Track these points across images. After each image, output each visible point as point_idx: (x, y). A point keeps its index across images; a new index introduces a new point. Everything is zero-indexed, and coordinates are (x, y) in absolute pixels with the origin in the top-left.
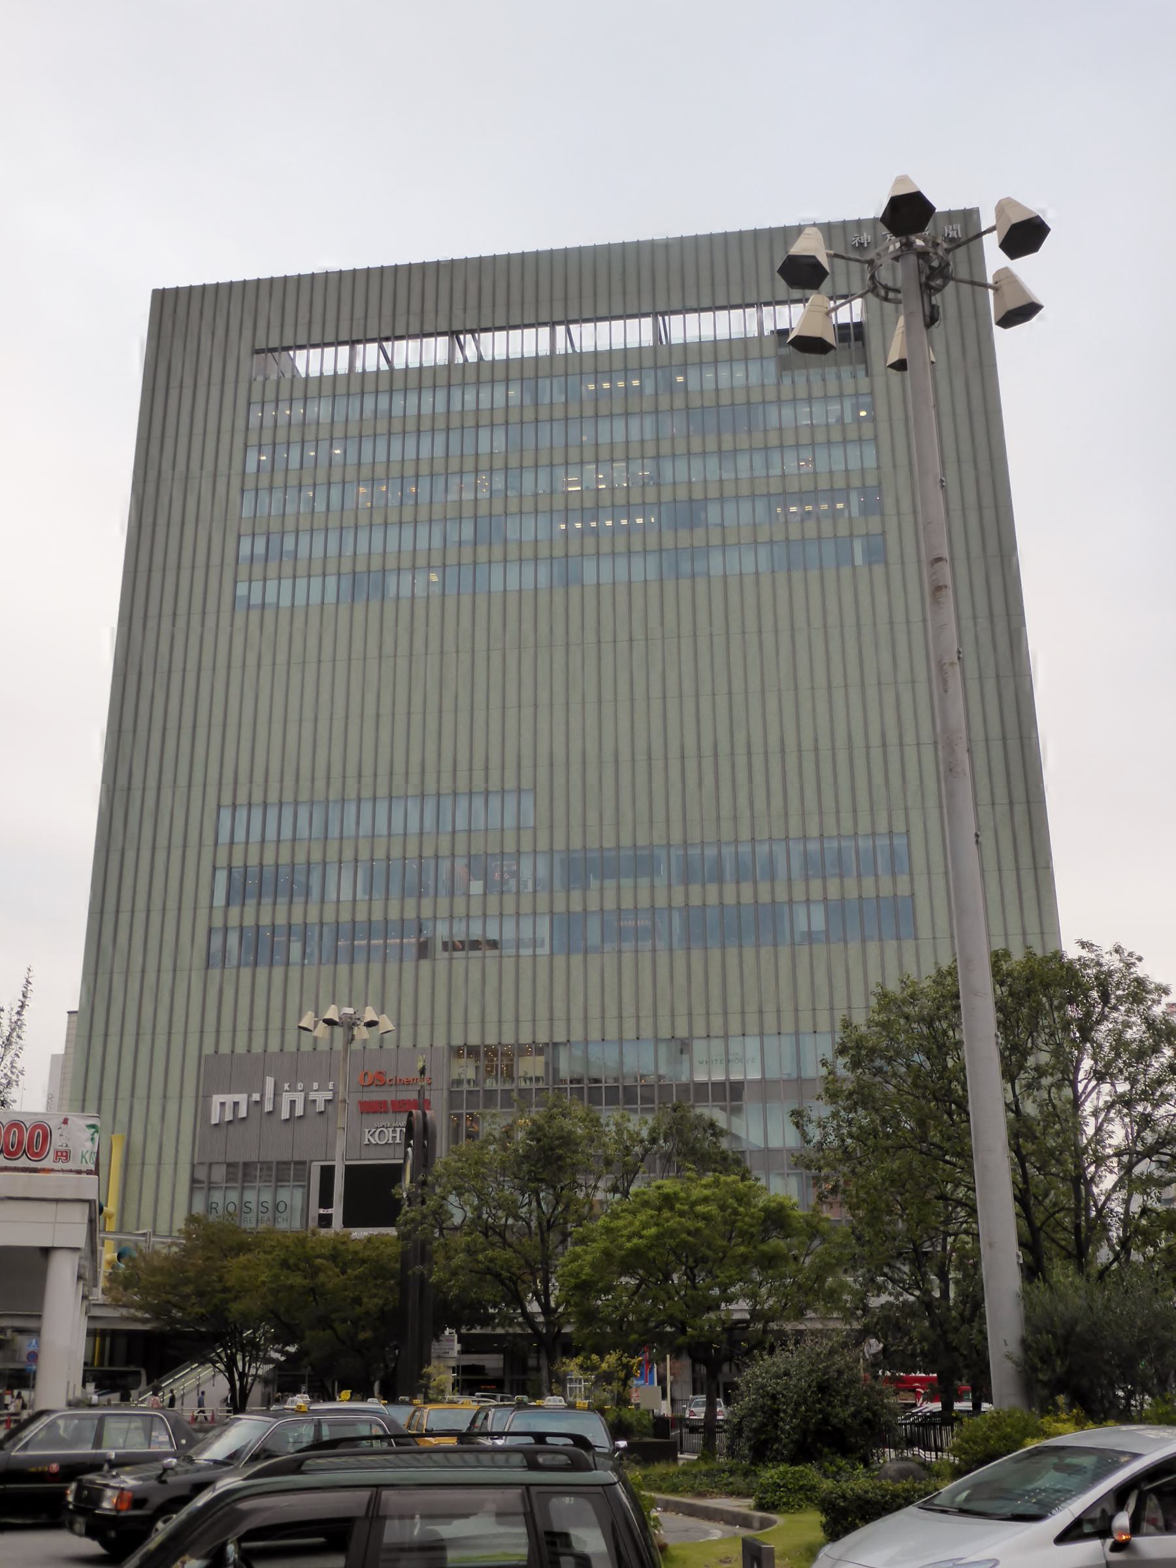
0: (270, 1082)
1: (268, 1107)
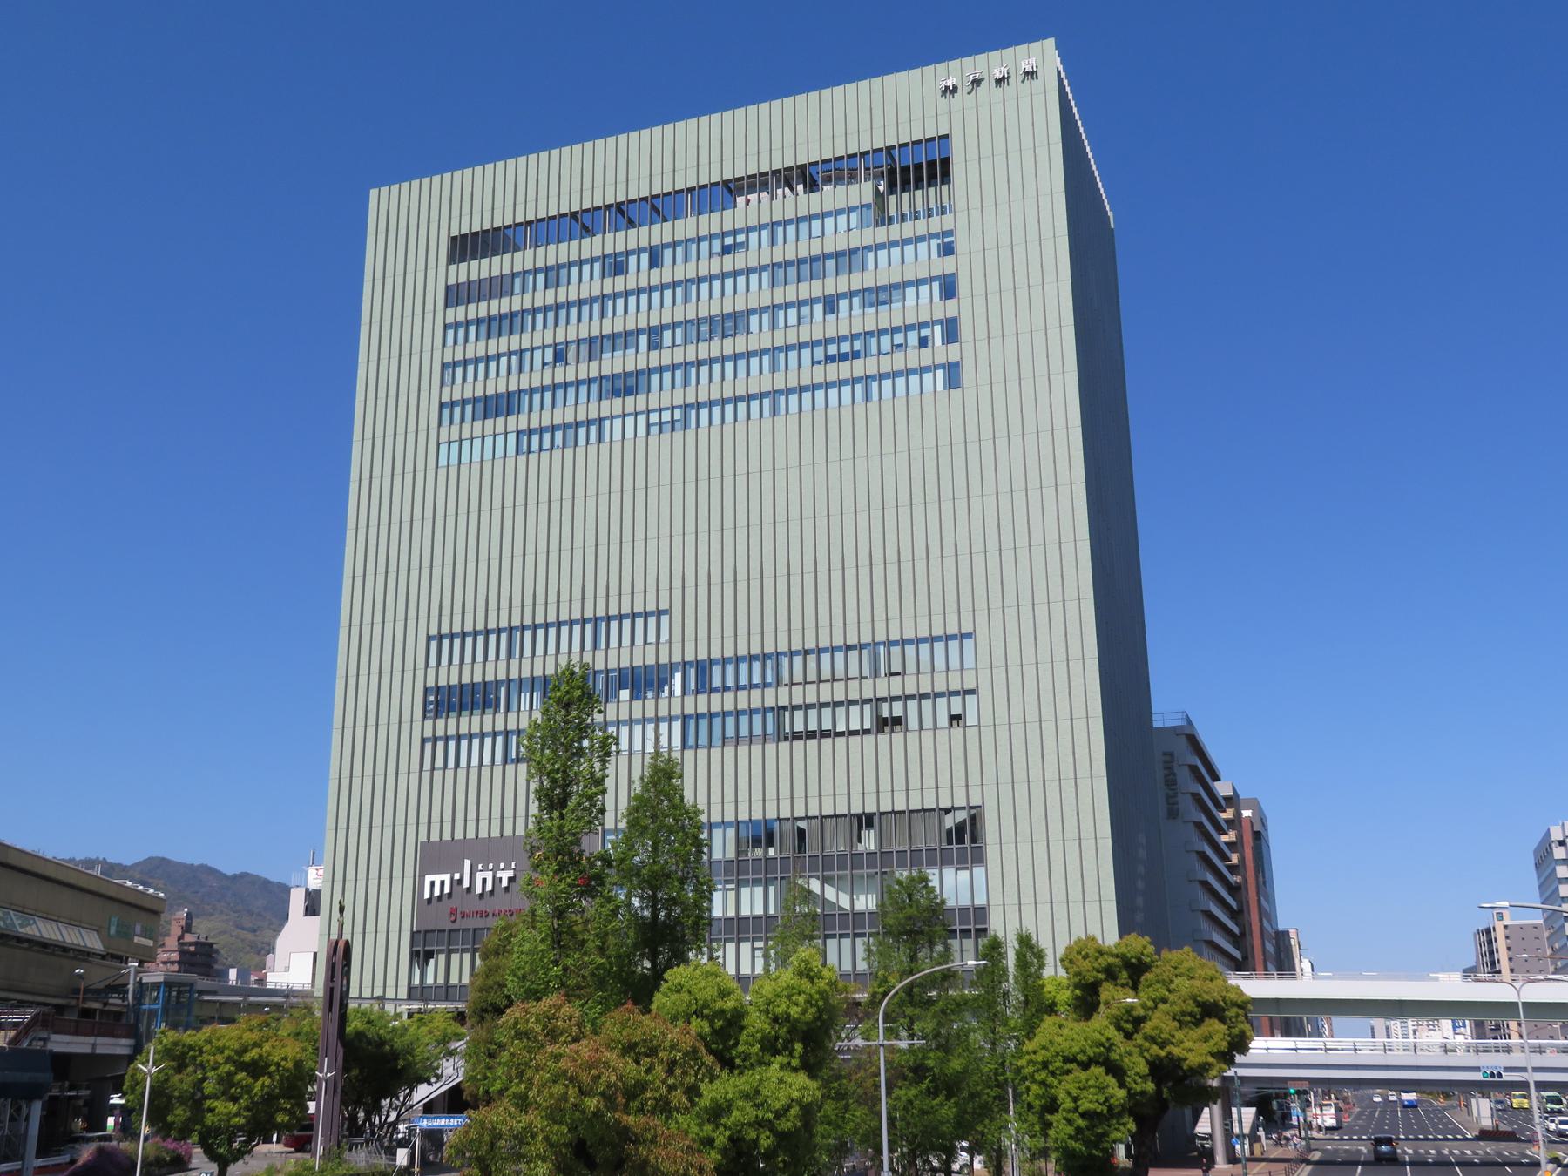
0: (467, 863)
1: (466, 884)
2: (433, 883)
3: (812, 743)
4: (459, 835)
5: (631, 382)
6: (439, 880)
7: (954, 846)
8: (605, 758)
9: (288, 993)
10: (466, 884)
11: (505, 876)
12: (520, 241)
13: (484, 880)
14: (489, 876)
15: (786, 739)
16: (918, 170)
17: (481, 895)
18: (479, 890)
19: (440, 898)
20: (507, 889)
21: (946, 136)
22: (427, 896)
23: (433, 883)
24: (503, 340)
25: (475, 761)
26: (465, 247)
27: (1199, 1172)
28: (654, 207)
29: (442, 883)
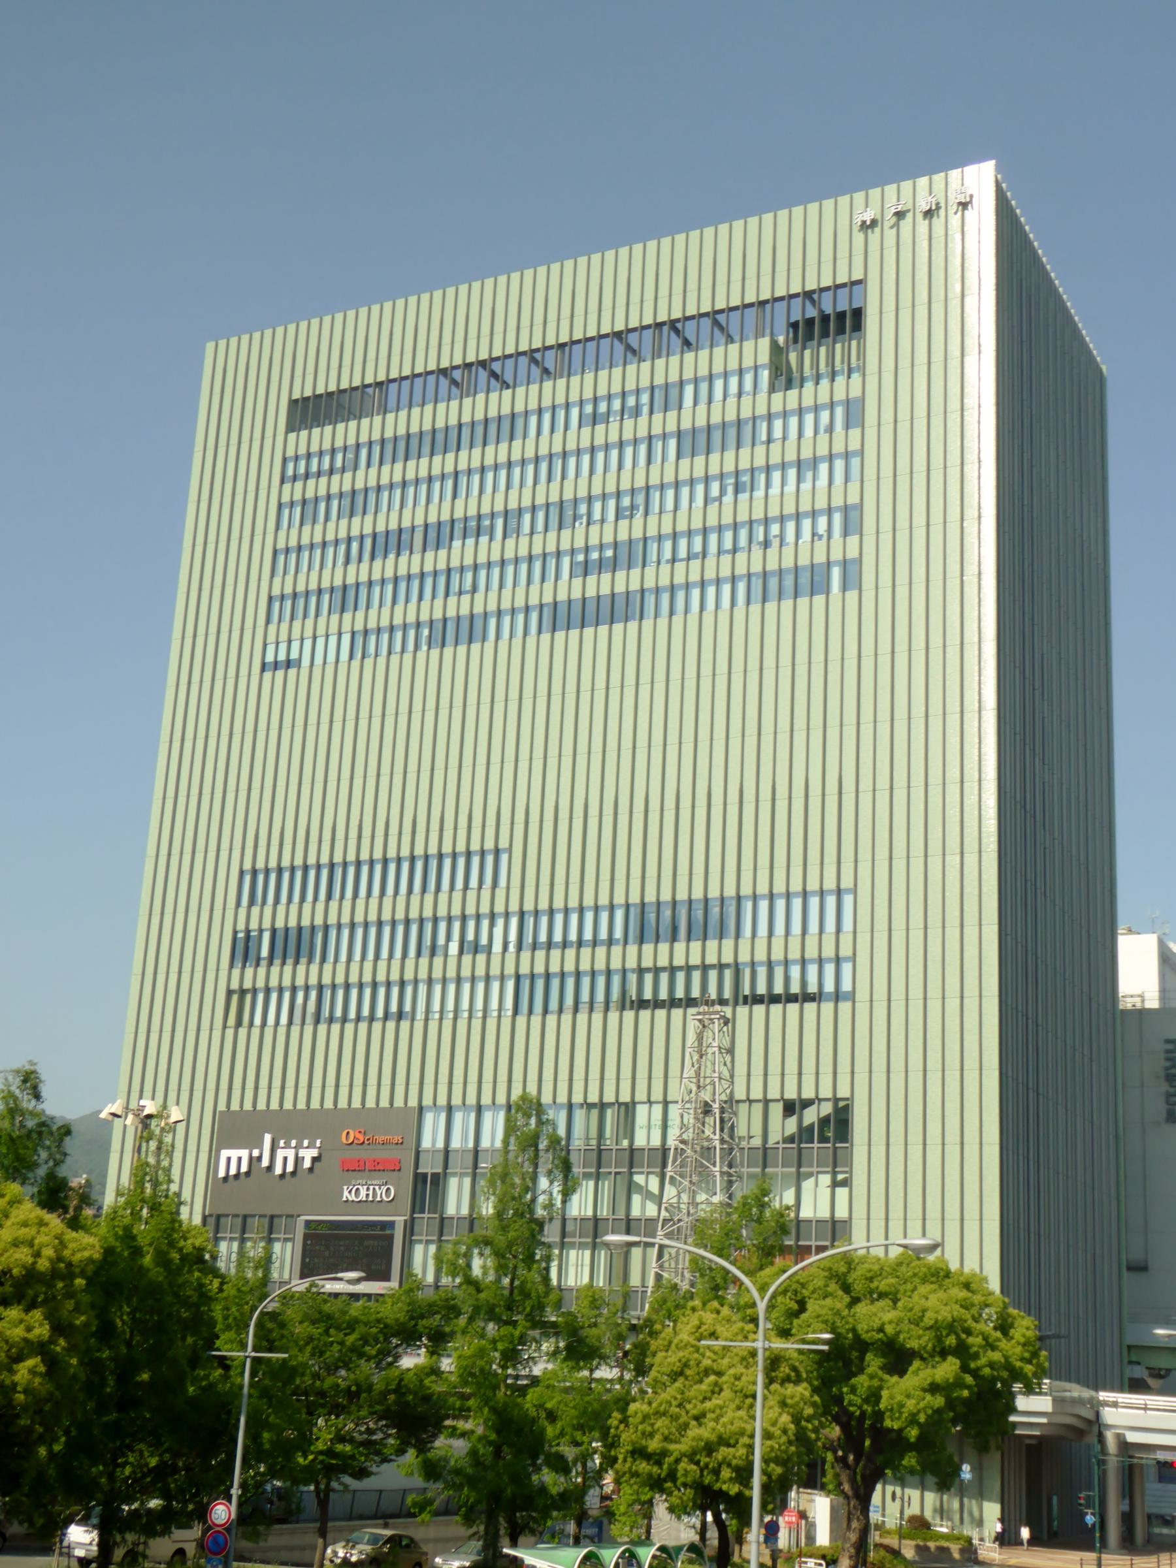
0: (268, 1138)
1: (265, 1162)
2: (229, 1159)
3: (793, 1008)
4: (370, 1103)
6: (235, 1158)
7: (816, 1145)
10: (265, 1162)
11: (308, 1155)
12: (734, 330)
13: (285, 1159)
14: (290, 1154)
15: (745, 1002)
16: (828, 322)
17: (282, 1176)
18: (278, 1170)
19: (237, 1176)
20: (311, 1169)
21: (859, 282)
22: (222, 1174)
23: (229, 1159)
24: (700, 460)
25: (258, 1021)
26: (309, 411)
27: (1091, 1556)
28: (716, 323)
29: (240, 1159)
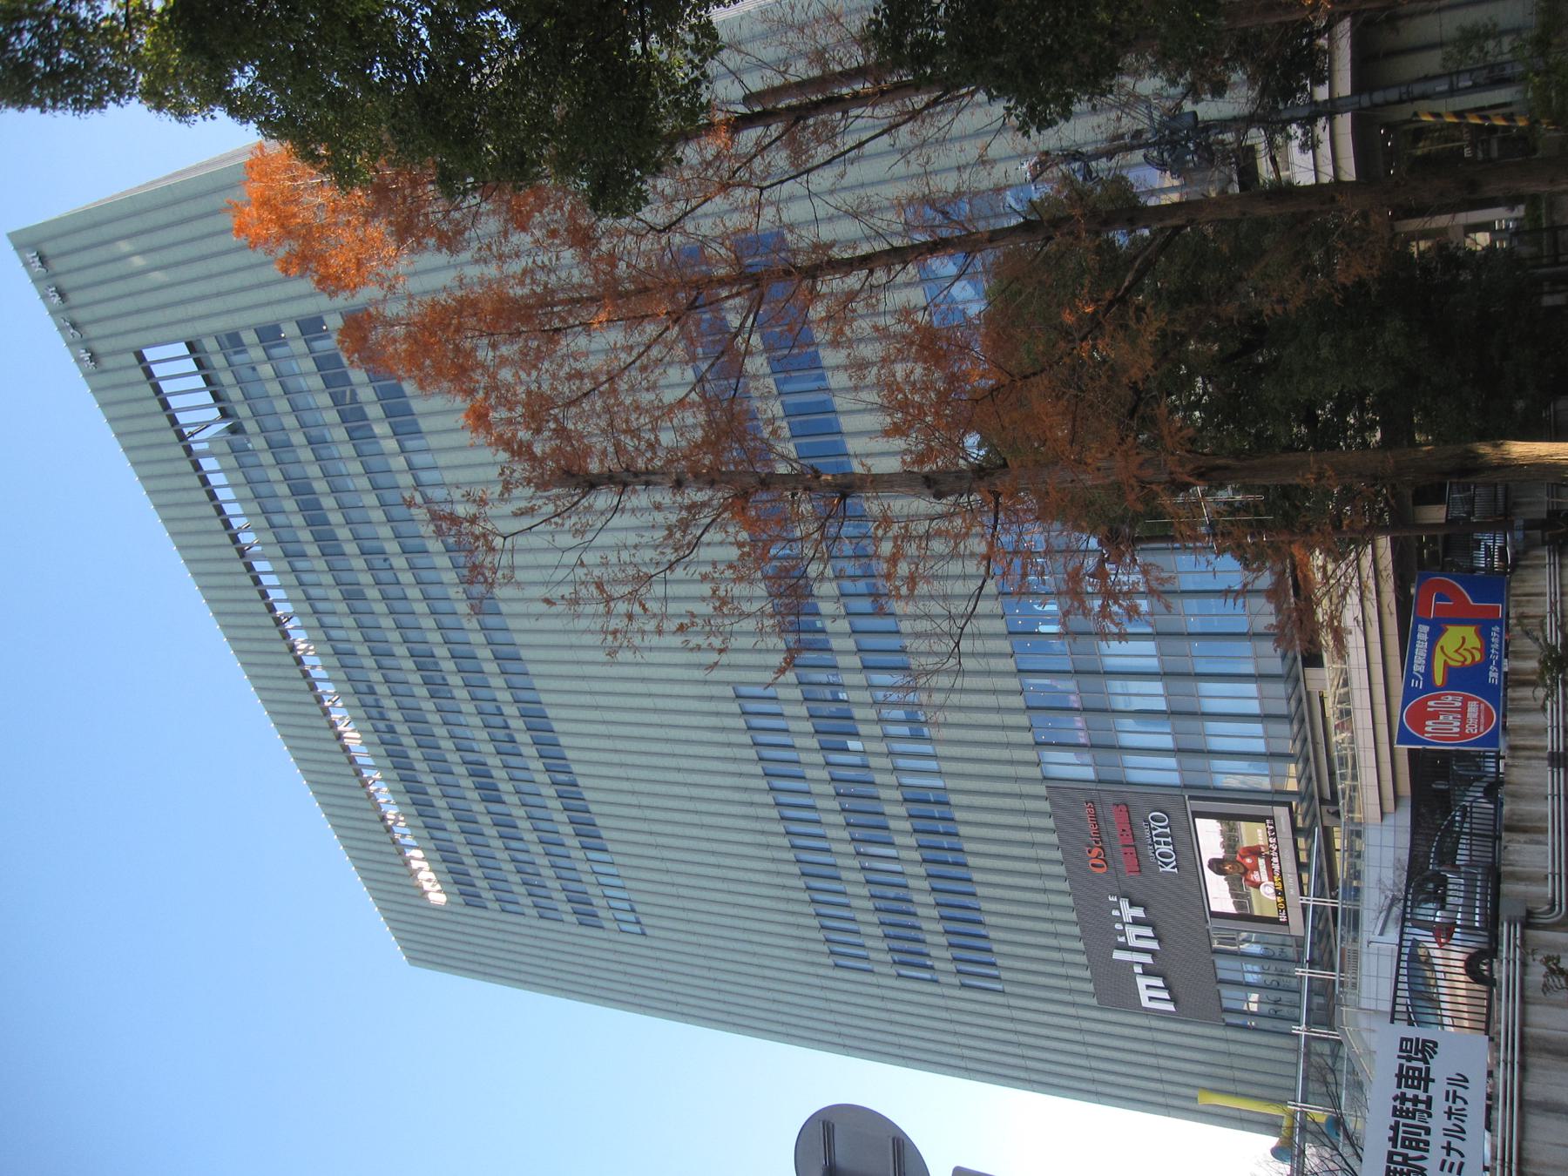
0: (1118, 955)
1: (1147, 959)
2: (1151, 999)
5: (363, 687)
8: (1122, 136)
9: (991, 297)
10: (1147, 959)
11: (1129, 912)
14: (1132, 931)
18: (1154, 945)
29: (1148, 987)
